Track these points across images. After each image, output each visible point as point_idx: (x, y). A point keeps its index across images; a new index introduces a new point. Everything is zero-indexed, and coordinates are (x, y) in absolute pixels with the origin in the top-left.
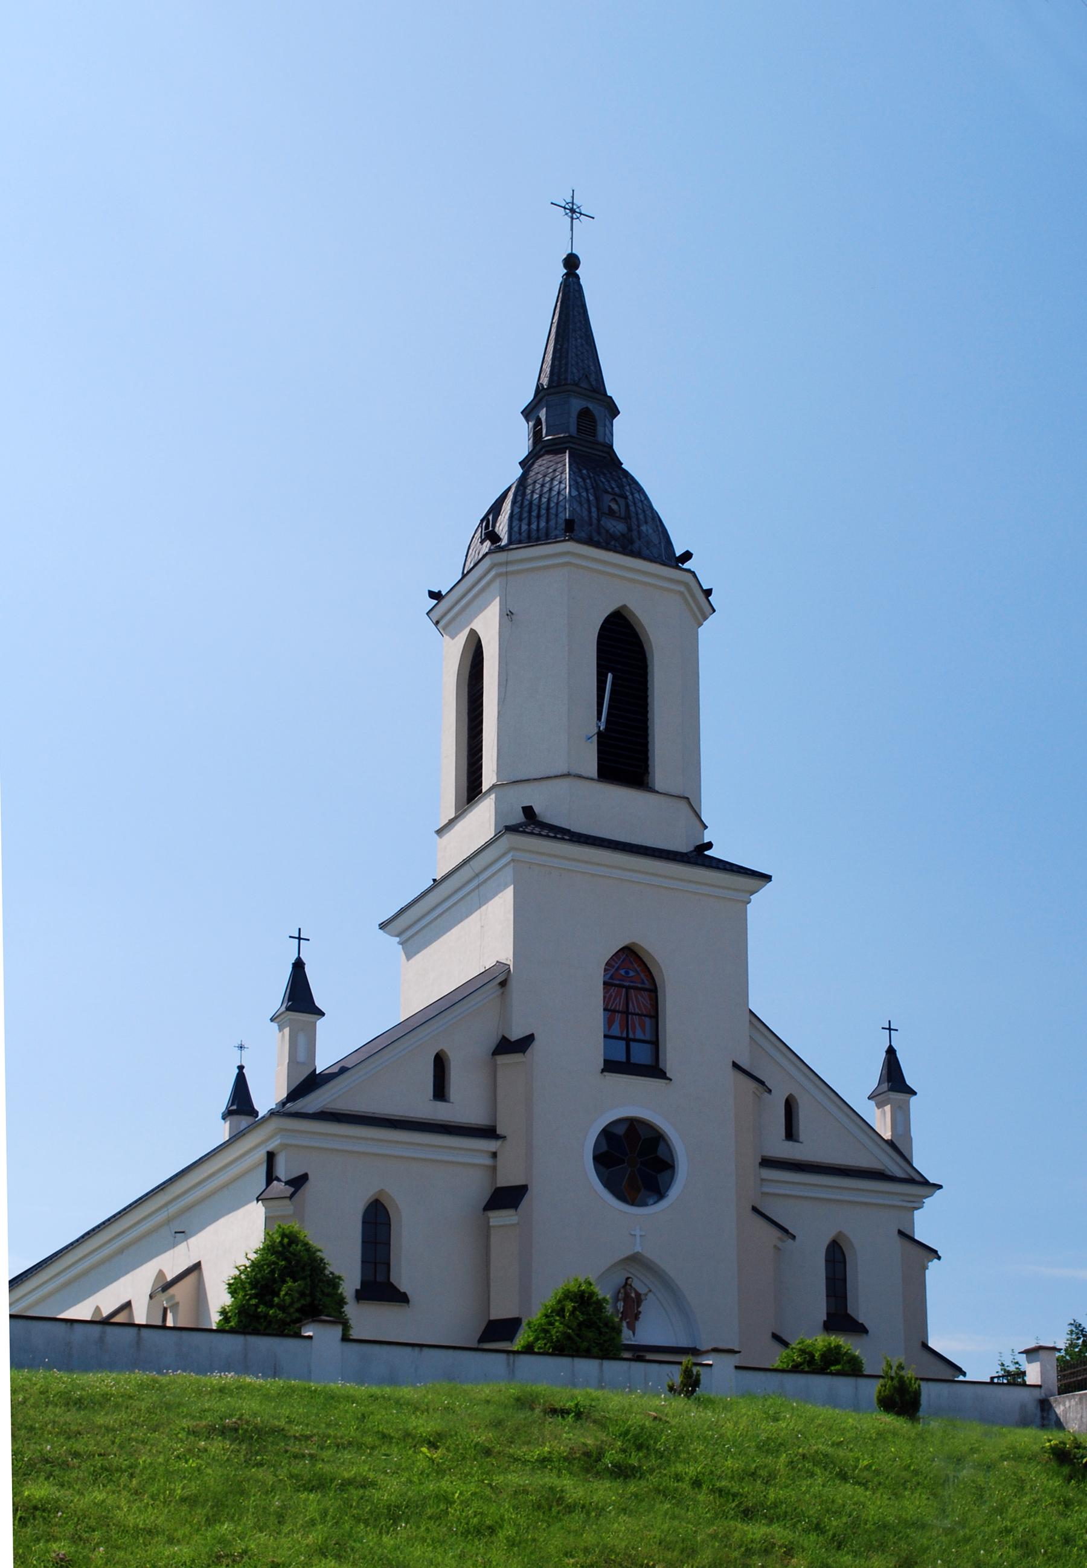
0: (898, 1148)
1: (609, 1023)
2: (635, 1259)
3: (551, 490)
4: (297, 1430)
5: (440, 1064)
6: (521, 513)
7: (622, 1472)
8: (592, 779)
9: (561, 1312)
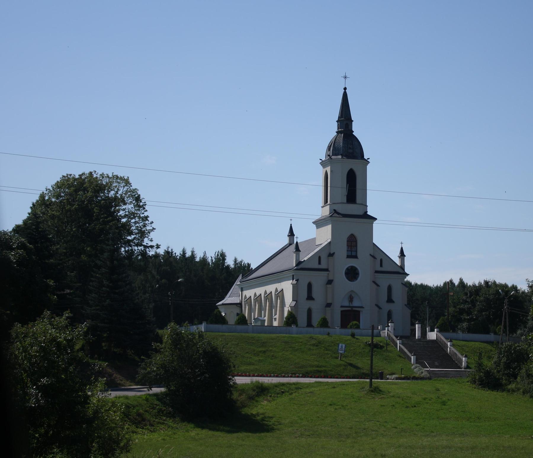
0: (402, 267)
1: (348, 248)
2: (352, 291)
3: (339, 144)
4: (290, 342)
5: (320, 258)
6: (334, 149)
7: (317, 346)
8: (345, 203)
9: (321, 320)
